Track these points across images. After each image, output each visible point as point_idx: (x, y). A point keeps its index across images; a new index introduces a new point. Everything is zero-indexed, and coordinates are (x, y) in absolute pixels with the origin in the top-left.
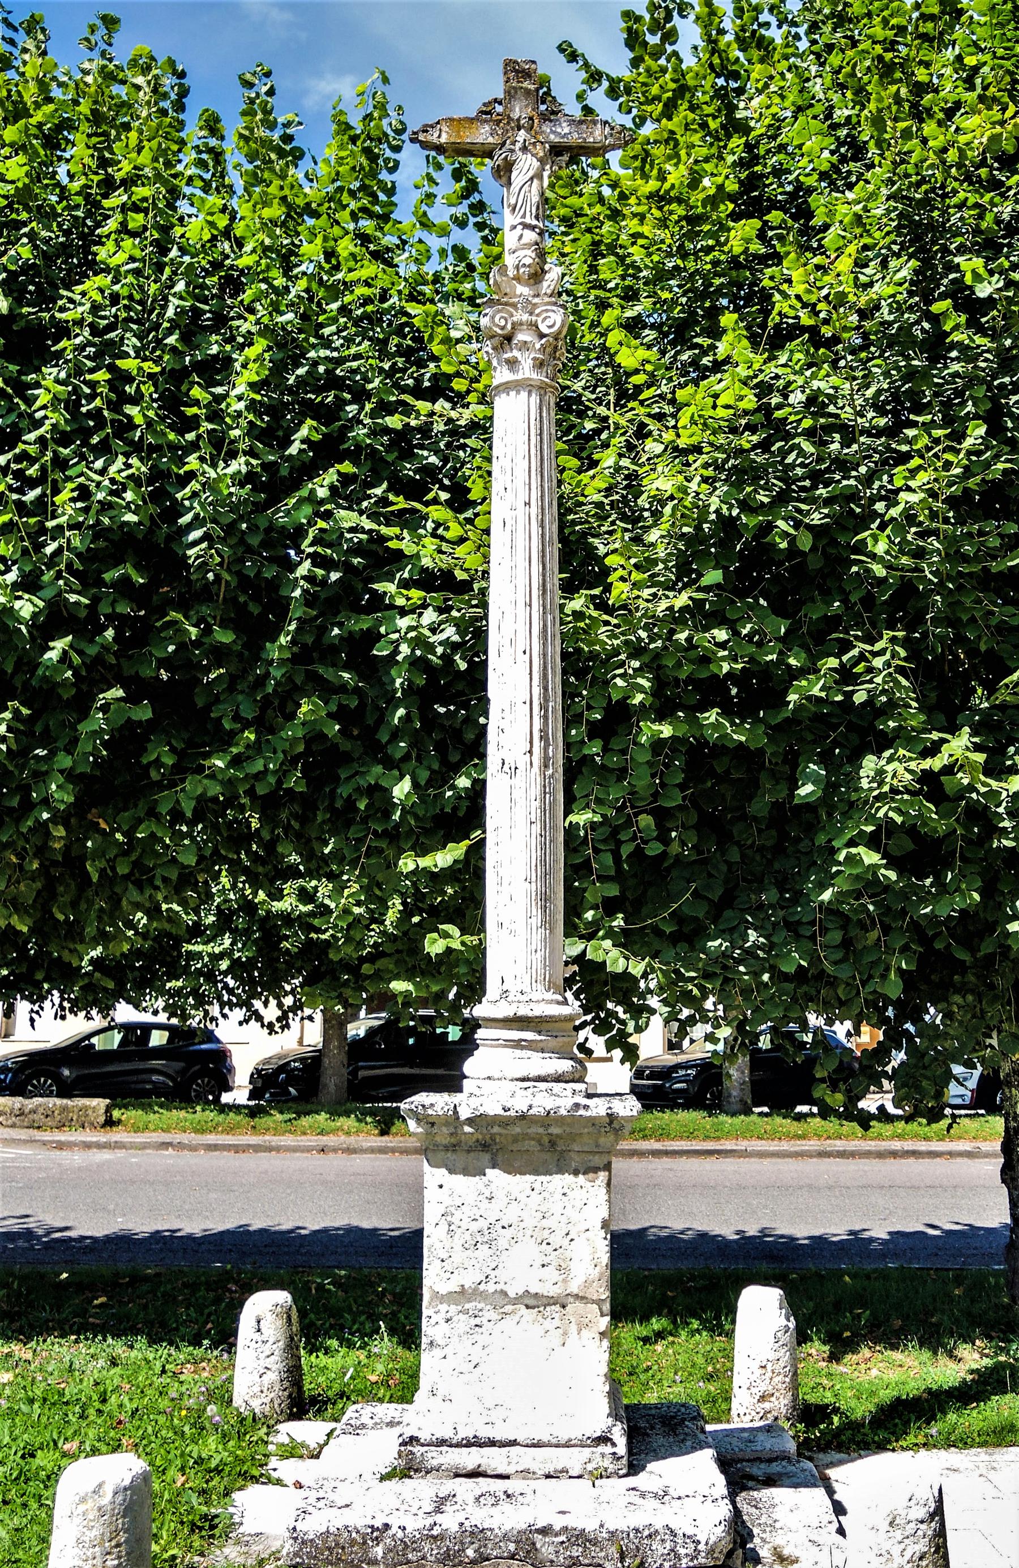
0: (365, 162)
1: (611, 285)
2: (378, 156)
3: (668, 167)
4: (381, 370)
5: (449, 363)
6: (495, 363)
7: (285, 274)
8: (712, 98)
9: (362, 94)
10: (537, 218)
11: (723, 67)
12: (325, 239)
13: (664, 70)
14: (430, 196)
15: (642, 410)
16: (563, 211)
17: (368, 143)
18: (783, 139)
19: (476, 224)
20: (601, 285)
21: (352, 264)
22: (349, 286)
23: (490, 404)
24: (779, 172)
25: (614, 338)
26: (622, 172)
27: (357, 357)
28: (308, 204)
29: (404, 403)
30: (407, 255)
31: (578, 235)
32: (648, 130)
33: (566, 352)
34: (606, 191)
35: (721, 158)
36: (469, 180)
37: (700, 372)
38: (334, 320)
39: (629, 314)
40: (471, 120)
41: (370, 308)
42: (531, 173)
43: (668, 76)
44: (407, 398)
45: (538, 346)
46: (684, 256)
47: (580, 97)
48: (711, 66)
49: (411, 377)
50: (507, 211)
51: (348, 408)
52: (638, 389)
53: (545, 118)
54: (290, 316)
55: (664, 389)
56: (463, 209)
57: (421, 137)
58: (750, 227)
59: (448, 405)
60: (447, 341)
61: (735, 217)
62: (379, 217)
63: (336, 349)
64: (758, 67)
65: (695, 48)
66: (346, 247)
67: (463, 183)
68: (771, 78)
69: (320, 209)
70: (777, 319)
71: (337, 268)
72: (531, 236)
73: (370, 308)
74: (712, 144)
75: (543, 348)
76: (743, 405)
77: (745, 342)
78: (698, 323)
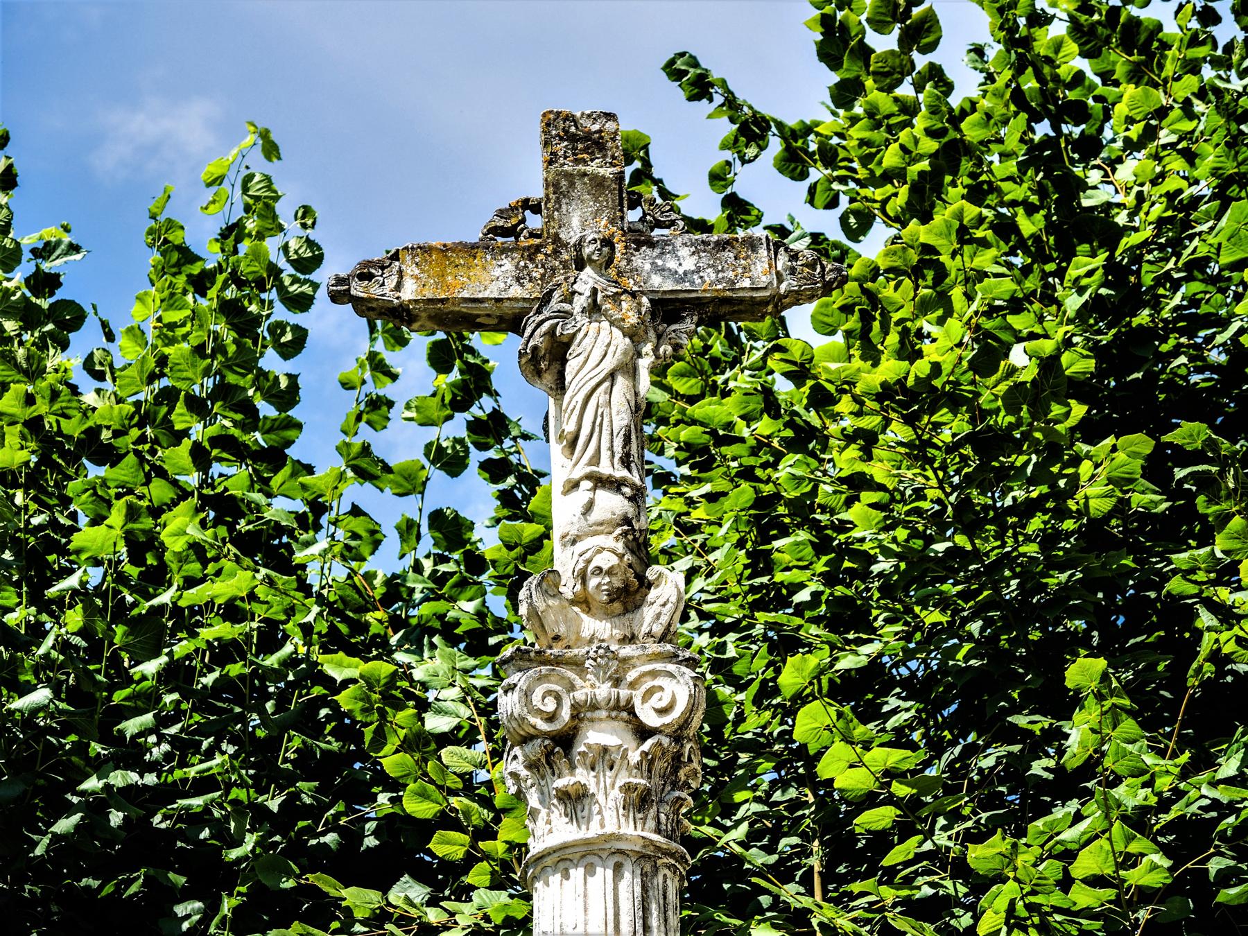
0: (229, 337)
1: (803, 596)
2: (256, 320)
3: (926, 324)
4: (261, 813)
5: (423, 795)
6: (533, 799)
7: (36, 599)
8: (1023, 167)
9: (218, 180)
10: (626, 462)
11: (1046, 95)
12: (132, 513)
13: (909, 109)
14: (378, 406)
15: (889, 894)
16: (686, 433)
17: (230, 293)
18: (1195, 248)
19: (486, 466)
20: (778, 598)
21: (194, 568)
22: (188, 620)
23: (528, 898)
24: (1193, 320)
25: (811, 722)
26: (820, 342)
27: (204, 784)
28: (93, 433)
29: (314, 892)
30: (323, 543)
31: (722, 485)
32: (874, 246)
33: (705, 762)
34: (783, 387)
35: (1049, 298)
36: (469, 369)
37: (1020, 801)
38: (148, 700)
39: (847, 662)
40: (471, 249)
41: (235, 669)
42: (609, 364)
43: (920, 122)
44: (327, 884)
45: (635, 757)
46: (972, 530)
47: (718, 178)
48: (1018, 97)
49: (332, 826)
50: (556, 449)
51: (180, 910)
52: (881, 841)
53: (639, 239)
54: (42, 695)
55: (941, 839)
56: (457, 427)
57: (358, 289)
58: (1128, 451)
59: (419, 892)
60: (423, 744)
61: (1091, 431)
62: (259, 455)
63: (154, 767)
64: (1129, 90)
65: (979, 51)
66: (180, 528)
67: (455, 376)
68: (1162, 113)
69: (119, 442)
70: (1209, 668)
71: (157, 577)
72: (611, 504)
73: (235, 669)
74: (1026, 271)
75: (648, 762)
76: (1135, 877)
77: (1129, 726)
78: (1017, 680)
